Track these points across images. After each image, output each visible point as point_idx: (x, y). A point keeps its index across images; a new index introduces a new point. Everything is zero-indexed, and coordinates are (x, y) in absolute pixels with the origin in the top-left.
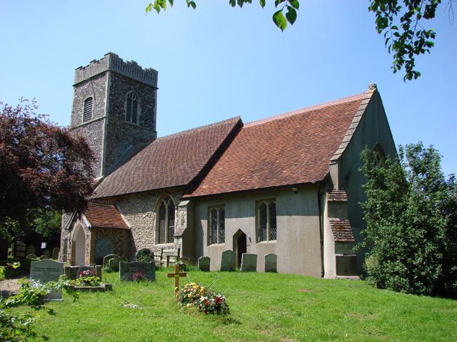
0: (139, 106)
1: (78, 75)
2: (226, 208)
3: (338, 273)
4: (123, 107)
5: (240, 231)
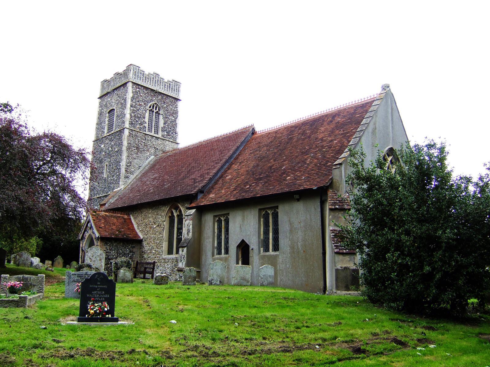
0: (161, 117)
1: (103, 88)
2: (230, 217)
3: (337, 288)
4: (144, 118)
5: (243, 241)
